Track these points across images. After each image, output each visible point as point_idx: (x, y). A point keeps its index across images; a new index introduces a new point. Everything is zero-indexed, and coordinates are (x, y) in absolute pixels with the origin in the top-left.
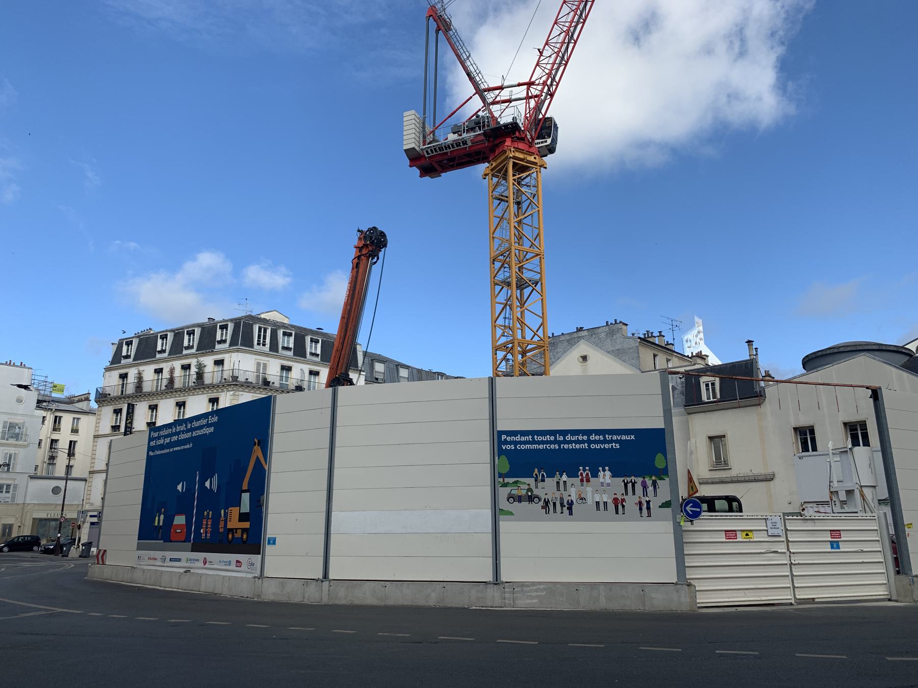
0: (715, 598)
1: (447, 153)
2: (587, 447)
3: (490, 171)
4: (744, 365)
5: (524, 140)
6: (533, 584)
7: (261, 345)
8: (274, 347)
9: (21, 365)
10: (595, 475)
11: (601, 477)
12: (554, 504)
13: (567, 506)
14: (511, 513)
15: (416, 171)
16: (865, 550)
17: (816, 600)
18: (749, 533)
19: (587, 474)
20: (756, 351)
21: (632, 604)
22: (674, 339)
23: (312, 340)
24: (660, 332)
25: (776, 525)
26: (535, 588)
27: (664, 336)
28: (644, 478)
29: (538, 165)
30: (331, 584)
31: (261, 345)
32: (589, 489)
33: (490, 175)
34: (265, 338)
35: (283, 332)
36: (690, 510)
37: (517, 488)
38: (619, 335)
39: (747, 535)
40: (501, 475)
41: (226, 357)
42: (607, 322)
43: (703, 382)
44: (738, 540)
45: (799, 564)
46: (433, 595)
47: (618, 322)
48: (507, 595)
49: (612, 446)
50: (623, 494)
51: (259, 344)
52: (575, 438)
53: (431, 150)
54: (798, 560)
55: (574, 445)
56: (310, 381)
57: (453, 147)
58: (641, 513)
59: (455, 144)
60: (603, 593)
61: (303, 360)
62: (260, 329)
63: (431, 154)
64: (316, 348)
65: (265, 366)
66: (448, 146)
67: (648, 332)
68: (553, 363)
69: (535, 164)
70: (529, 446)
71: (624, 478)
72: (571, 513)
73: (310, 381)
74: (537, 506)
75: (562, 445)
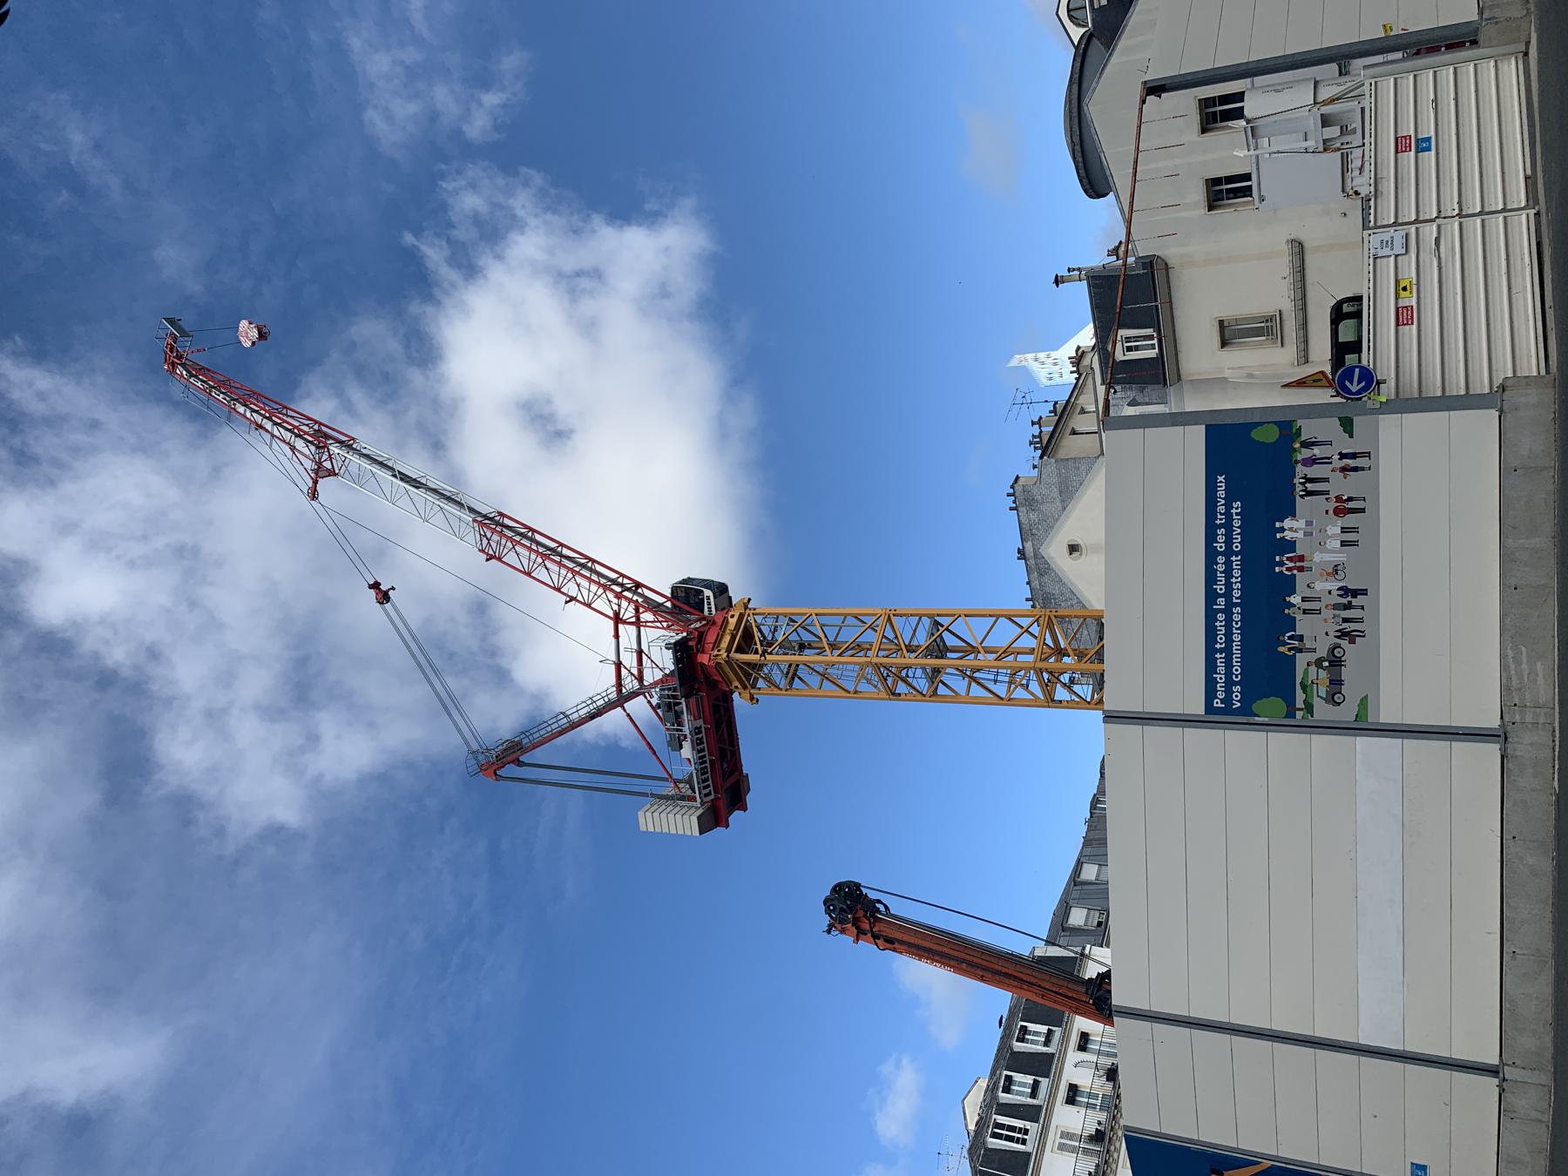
3: (747, 691)
4: (1096, 290)
5: (703, 633)
6: (1504, 667)
7: (1025, 1137)
8: (1031, 1113)
10: (1291, 545)
12: (1346, 620)
13: (1349, 599)
14: (1364, 702)
15: (736, 817)
16: (1432, 96)
17: (1529, 172)
19: (1288, 559)
20: (1074, 270)
22: (1046, 401)
23: (1021, 1039)
24: (1033, 423)
25: (1387, 241)
26: (1512, 666)
27: (1041, 418)
28: (1297, 462)
30: (1510, 1063)
31: (1025, 1137)
33: (752, 691)
34: (1012, 1128)
36: (1359, 383)
38: (1035, 491)
40: (1291, 714)
42: (1011, 509)
44: (1414, 303)
46: (1530, 860)
47: (1012, 491)
48: (1529, 718)
49: (1237, 514)
50: (1327, 499)
51: (1024, 1142)
52: (1221, 577)
53: (705, 788)
54: (1452, 203)
55: (1234, 580)
56: (1099, 1053)
57: (703, 750)
58: (1363, 469)
60: (1521, 541)
62: (995, 1135)
63: (711, 788)
64: (1036, 1033)
65: (1065, 1135)
67: (1031, 443)
68: (1080, 602)
69: (741, 616)
72: (1364, 592)
73: (1099, 1053)
74: (1350, 651)
75: (1235, 601)
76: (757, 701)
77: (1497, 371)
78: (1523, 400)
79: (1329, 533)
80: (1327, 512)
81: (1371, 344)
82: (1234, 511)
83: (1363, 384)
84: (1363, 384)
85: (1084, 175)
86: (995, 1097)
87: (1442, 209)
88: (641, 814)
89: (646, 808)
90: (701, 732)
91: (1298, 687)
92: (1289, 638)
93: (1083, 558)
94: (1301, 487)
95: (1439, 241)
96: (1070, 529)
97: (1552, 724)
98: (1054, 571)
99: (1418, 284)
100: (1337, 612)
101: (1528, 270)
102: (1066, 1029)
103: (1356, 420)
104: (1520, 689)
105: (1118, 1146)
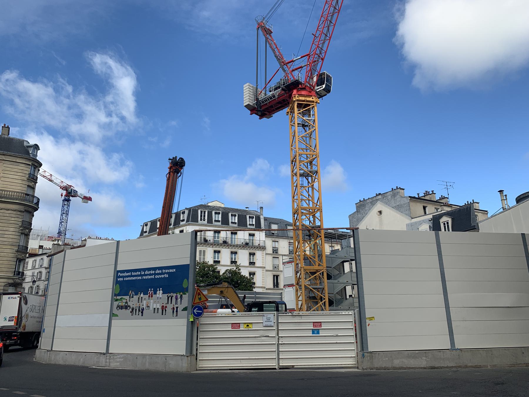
0: (209, 365)
1: (266, 104)
2: (154, 278)
5: (305, 89)
6: (119, 354)
7: (203, 220)
8: (210, 221)
9: (112, 239)
10: (155, 293)
11: (158, 294)
12: (136, 310)
13: (141, 311)
14: (117, 316)
15: (256, 117)
16: (339, 335)
17: (295, 367)
18: (249, 325)
19: (152, 292)
20: (506, 197)
21: (160, 367)
22: (448, 194)
24: (433, 191)
25: (270, 320)
26: (119, 356)
28: (177, 294)
29: (315, 102)
31: (203, 220)
32: (152, 301)
34: (204, 216)
35: (215, 212)
36: (196, 312)
37: (121, 302)
38: (398, 196)
39: (248, 326)
41: (184, 228)
43: (442, 222)
44: (241, 329)
45: (284, 344)
48: (108, 360)
49: (165, 276)
50: (166, 303)
51: (201, 220)
52: (149, 272)
54: (284, 341)
55: (148, 276)
56: (232, 238)
58: (173, 314)
59: (269, 98)
60: (148, 360)
61: (227, 227)
62: (201, 212)
64: (235, 219)
66: (268, 99)
67: (426, 191)
68: (364, 217)
69: (313, 102)
70: (132, 278)
71: (168, 294)
72: (142, 315)
73: (232, 238)
74: (128, 311)
75: (143, 277)
76: (288, 115)
77: (208, 355)
78: (184, 362)
79: (158, 305)
80: (163, 304)
81: (250, 315)
82: (166, 275)
83: (196, 314)
84: (196, 314)
85: (521, 198)
86: (213, 210)
87: (283, 338)
88: (248, 84)
89: (251, 85)
90: (274, 98)
91: (121, 297)
92: (133, 294)
93: (378, 216)
94: (170, 295)
95: (268, 337)
96: (387, 211)
97: (106, 367)
98: (373, 207)
99: (248, 330)
100: (138, 307)
101: (251, 365)
102: (237, 227)
103: (186, 312)
104: (114, 358)
105: (204, 246)
